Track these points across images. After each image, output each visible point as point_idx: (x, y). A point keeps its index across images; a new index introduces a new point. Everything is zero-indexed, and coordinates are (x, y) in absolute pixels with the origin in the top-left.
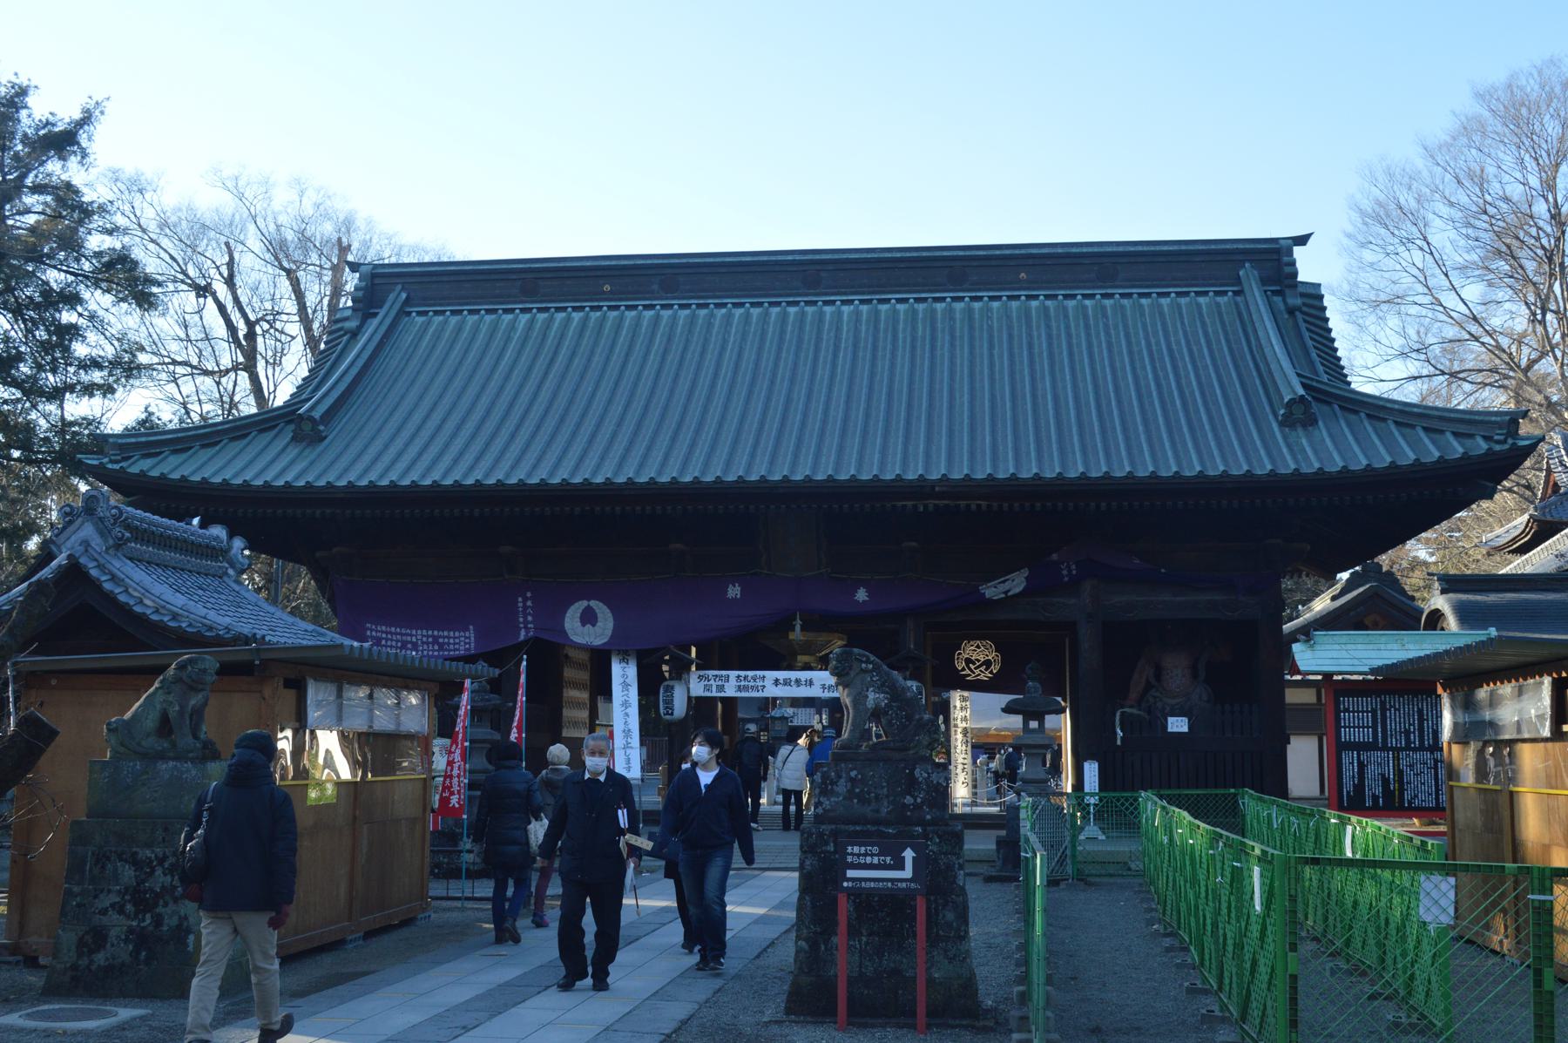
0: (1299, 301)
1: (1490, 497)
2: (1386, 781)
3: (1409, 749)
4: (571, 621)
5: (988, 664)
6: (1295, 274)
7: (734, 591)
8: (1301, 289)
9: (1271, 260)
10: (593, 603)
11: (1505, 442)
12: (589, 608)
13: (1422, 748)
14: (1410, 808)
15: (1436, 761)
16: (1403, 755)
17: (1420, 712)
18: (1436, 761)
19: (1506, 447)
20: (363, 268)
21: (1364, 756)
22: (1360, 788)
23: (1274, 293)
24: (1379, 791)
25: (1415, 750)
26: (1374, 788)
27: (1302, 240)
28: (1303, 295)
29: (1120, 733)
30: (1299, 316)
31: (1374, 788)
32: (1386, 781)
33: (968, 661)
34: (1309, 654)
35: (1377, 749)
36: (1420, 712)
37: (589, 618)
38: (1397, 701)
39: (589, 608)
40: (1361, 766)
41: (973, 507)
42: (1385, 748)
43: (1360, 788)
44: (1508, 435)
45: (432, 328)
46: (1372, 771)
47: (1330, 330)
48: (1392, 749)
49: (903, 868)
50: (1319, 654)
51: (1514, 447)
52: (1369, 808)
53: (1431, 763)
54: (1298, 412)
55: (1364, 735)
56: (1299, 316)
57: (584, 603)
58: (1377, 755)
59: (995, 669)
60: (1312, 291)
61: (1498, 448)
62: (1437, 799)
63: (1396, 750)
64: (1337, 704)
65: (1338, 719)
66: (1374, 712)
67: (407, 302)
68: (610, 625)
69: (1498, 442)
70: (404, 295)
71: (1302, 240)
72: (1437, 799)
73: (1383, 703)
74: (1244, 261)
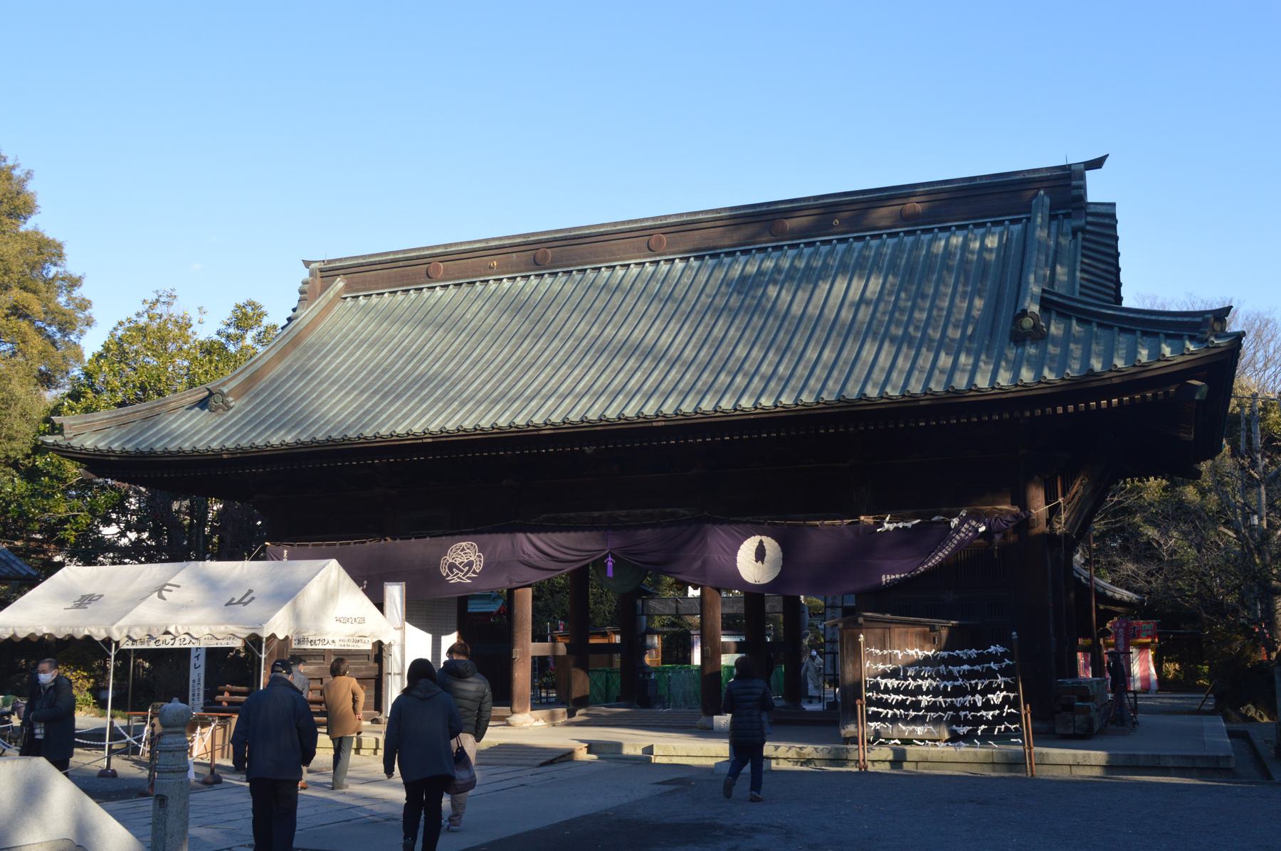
5: (470, 564)
10: (764, 538)
27: (1097, 164)
30: (1080, 235)
33: (452, 567)
37: (760, 554)
39: (761, 542)
71: (1097, 164)
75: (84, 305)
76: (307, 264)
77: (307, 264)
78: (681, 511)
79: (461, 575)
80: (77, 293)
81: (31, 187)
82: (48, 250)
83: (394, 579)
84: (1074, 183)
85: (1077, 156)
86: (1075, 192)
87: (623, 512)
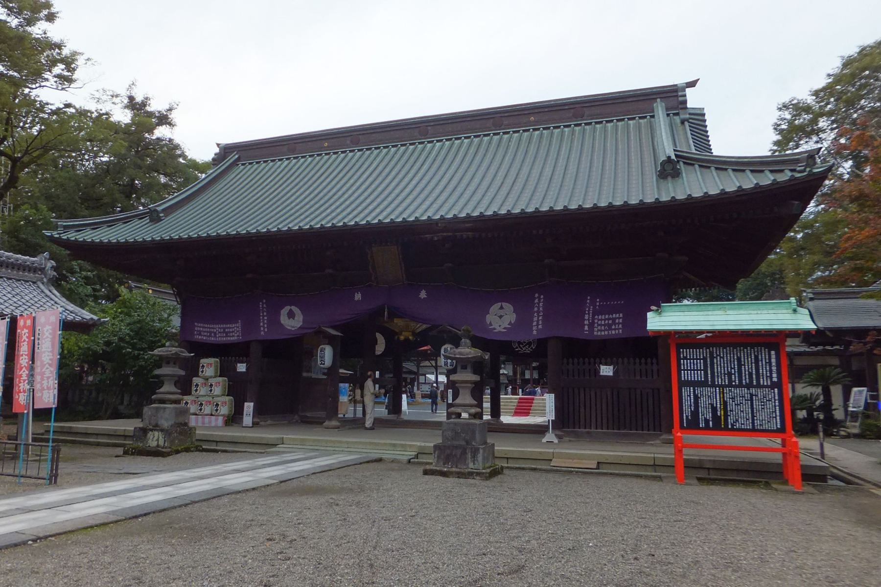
0: (688, 116)
2: (714, 410)
3: (732, 386)
4: (284, 319)
6: (685, 102)
7: (358, 296)
9: (672, 97)
10: (294, 308)
11: (804, 171)
12: (291, 310)
13: (740, 385)
14: (733, 429)
15: (752, 395)
16: (726, 390)
17: (739, 359)
18: (752, 395)
21: (698, 391)
22: (695, 413)
24: (709, 416)
25: (736, 387)
26: (705, 414)
27: (692, 84)
28: (690, 114)
29: (838, 347)
30: (686, 124)
31: (705, 414)
32: (714, 410)
34: (658, 318)
35: (708, 386)
36: (739, 359)
37: (291, 315)
38: (722, 352)
39: (291, 310)
40: (696, 398)
41: (465, 236)
42: (713, 385)
43: (695, 413)
45: (244, 173)
46: (703, 401)
47: (708, 137)
48: (719, 386)
50: (663, 319)
52: (702, 429)
53: (748, 396)
54: (669, 168)
55: (699, 376)
58: (707, 391)
60: (699, 112)
61: (798, 175)
62: (753, 423)
63: (722, 386)
64: (678, 353)
65: (679, 365)
66: (705, 359)
67: (238, 159)
68: (301, 318)
69: (800, 172)
71: (692, 84)
72: (753, 423)
73: (711, 354)
76: (218, 145)
77: (218, 145)
84: (680, 94)
86: (680, 99)
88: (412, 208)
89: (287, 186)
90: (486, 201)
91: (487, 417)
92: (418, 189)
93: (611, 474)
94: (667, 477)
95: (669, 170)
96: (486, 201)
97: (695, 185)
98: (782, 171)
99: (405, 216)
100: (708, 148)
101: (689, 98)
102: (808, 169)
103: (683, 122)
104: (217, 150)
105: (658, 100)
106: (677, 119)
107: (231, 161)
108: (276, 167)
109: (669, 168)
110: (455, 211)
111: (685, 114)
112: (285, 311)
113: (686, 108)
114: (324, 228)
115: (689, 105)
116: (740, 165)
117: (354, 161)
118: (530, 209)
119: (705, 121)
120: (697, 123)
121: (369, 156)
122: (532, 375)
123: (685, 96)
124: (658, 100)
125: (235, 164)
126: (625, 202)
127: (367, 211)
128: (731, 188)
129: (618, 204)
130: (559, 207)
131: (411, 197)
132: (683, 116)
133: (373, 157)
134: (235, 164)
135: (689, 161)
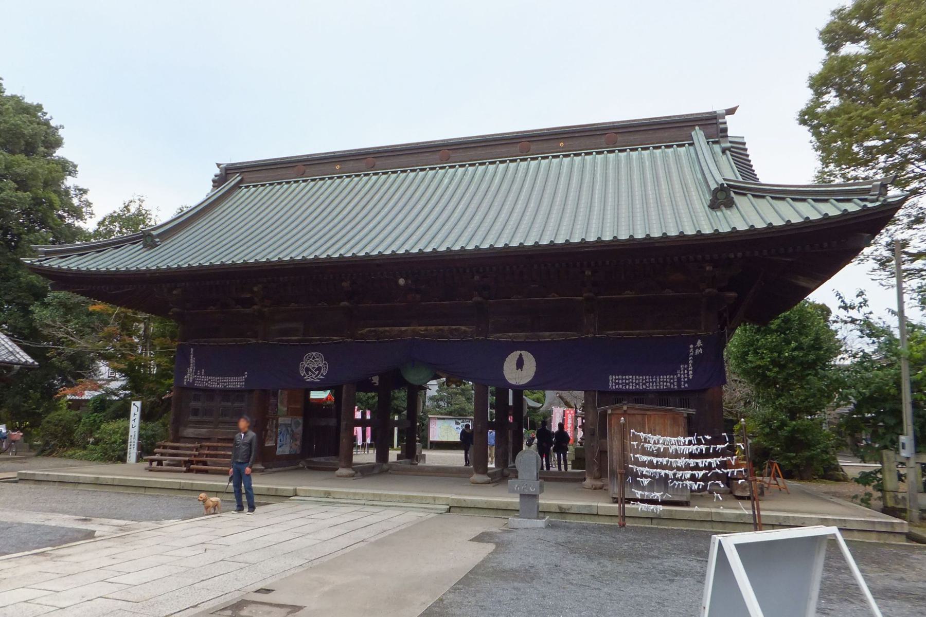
0: (729, 145)
1: (869, 245)
5: (319, 369)
6: (725, 130)
8: (730, 139)
9: (712, 125)
10: (523, 352)
11: (877, 200)
19: (878, 204)
20: (873, 386)
23: (714, 142)
27: (731, 111)
28: (731, 142)
30: (728, 152)
33: (307, 370)
37: (520, 364)
39: (521, 355)
44: (880, 194)
45: (248, 196)
47: (751, 166)
49: (573, 468)
51: (885, 204)
56: (728, 152)
57: (519, 352)
59: (324, 372)
61: (870, 205)
67: (241, 181)
69: (872, 201)
70: (239, 178)
71: (731, 111)
74: (694, 126)
75: (89, 204)
76: (218, 165)
77: (218, 165)
78: (463, 328)
79: (313, 376)
80: (85, 197)
81: (61, 132)
82: (67, 168)
83: (309, 394)
84: (721, 121)
85: (719, 108)
86: (722, 126)
87: (423, 328)
88: (389, 240)
89: (645, 197)
90: (467, 235)
91: (545, 469)
92: (421, 218)
93: (62, 482)
94: (308, 494)
95: (722, 198)
96: (467, 235)
97: (748, 216)
98: (849, 201)
99: (355, 251)
100: (753, 176)
101: (729, 125)
102: (882, 199)
103: (724, 152)
104: (217, 171)
105: (697, 128)
106: (717, 148)
107: (233, 183)
108: (274, 191)
109: (721, 196)
110: (420, 246)
111: (726, 142)
112: (512, 358)
113: (727, 136)
114: (294, 260)
115: (729, 133)
116: (779, 193)
117: (368, 186)
118: (500, 245)
119: (746, 150)
120: (738, 153)
121: (367, 182)
122: (364, 414)
123: (725, 123)
124: (697, 128)
125: (237, 186)
126: (615, 237)
127: (328, 244)
128: (814, 216)
129: (607, 239)
130: (545, 242)
131: (286, 231)
132: (724, 145)
133: (361, 184)
134: (237, 186)
135: (742, 191)
